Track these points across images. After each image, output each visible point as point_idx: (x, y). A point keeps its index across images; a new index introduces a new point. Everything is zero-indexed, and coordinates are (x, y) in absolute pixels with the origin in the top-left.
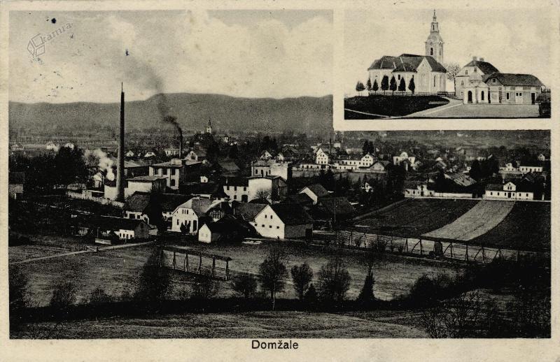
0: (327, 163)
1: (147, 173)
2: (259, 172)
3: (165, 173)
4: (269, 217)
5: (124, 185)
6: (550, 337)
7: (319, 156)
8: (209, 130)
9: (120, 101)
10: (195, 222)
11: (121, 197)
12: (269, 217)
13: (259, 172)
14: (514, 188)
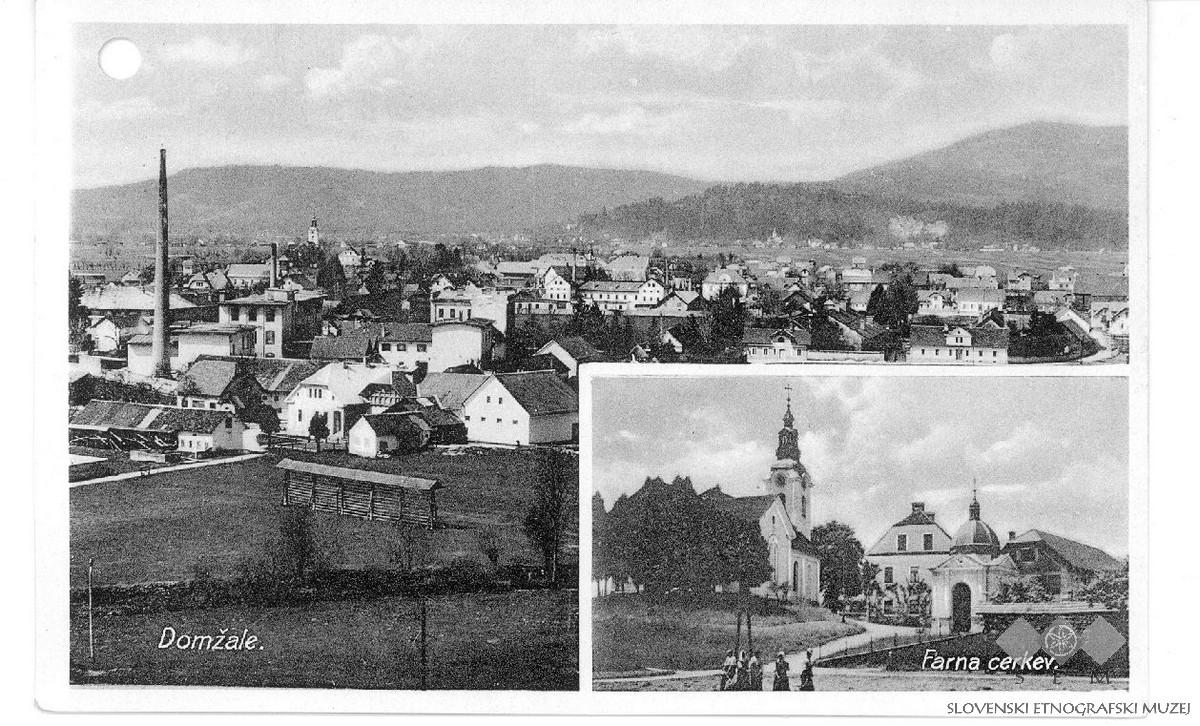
0: (568, 299)
1: (215, 318)
2: (447, 315)
3: (253, 317)
4: (495, 400)
5: (169, 347)
6: (577, 689)
7: (553, 285)
8: (314, 238)
9: (156, 175)
10: (337, 414)
11: (164, 371)
12: (495, 400)
13: (447, 315)
14: (967, 341)
